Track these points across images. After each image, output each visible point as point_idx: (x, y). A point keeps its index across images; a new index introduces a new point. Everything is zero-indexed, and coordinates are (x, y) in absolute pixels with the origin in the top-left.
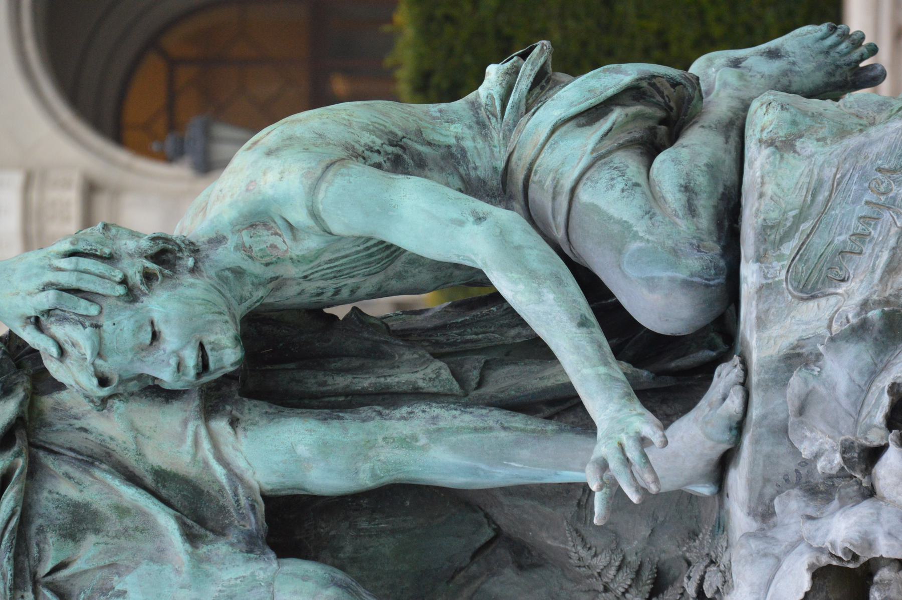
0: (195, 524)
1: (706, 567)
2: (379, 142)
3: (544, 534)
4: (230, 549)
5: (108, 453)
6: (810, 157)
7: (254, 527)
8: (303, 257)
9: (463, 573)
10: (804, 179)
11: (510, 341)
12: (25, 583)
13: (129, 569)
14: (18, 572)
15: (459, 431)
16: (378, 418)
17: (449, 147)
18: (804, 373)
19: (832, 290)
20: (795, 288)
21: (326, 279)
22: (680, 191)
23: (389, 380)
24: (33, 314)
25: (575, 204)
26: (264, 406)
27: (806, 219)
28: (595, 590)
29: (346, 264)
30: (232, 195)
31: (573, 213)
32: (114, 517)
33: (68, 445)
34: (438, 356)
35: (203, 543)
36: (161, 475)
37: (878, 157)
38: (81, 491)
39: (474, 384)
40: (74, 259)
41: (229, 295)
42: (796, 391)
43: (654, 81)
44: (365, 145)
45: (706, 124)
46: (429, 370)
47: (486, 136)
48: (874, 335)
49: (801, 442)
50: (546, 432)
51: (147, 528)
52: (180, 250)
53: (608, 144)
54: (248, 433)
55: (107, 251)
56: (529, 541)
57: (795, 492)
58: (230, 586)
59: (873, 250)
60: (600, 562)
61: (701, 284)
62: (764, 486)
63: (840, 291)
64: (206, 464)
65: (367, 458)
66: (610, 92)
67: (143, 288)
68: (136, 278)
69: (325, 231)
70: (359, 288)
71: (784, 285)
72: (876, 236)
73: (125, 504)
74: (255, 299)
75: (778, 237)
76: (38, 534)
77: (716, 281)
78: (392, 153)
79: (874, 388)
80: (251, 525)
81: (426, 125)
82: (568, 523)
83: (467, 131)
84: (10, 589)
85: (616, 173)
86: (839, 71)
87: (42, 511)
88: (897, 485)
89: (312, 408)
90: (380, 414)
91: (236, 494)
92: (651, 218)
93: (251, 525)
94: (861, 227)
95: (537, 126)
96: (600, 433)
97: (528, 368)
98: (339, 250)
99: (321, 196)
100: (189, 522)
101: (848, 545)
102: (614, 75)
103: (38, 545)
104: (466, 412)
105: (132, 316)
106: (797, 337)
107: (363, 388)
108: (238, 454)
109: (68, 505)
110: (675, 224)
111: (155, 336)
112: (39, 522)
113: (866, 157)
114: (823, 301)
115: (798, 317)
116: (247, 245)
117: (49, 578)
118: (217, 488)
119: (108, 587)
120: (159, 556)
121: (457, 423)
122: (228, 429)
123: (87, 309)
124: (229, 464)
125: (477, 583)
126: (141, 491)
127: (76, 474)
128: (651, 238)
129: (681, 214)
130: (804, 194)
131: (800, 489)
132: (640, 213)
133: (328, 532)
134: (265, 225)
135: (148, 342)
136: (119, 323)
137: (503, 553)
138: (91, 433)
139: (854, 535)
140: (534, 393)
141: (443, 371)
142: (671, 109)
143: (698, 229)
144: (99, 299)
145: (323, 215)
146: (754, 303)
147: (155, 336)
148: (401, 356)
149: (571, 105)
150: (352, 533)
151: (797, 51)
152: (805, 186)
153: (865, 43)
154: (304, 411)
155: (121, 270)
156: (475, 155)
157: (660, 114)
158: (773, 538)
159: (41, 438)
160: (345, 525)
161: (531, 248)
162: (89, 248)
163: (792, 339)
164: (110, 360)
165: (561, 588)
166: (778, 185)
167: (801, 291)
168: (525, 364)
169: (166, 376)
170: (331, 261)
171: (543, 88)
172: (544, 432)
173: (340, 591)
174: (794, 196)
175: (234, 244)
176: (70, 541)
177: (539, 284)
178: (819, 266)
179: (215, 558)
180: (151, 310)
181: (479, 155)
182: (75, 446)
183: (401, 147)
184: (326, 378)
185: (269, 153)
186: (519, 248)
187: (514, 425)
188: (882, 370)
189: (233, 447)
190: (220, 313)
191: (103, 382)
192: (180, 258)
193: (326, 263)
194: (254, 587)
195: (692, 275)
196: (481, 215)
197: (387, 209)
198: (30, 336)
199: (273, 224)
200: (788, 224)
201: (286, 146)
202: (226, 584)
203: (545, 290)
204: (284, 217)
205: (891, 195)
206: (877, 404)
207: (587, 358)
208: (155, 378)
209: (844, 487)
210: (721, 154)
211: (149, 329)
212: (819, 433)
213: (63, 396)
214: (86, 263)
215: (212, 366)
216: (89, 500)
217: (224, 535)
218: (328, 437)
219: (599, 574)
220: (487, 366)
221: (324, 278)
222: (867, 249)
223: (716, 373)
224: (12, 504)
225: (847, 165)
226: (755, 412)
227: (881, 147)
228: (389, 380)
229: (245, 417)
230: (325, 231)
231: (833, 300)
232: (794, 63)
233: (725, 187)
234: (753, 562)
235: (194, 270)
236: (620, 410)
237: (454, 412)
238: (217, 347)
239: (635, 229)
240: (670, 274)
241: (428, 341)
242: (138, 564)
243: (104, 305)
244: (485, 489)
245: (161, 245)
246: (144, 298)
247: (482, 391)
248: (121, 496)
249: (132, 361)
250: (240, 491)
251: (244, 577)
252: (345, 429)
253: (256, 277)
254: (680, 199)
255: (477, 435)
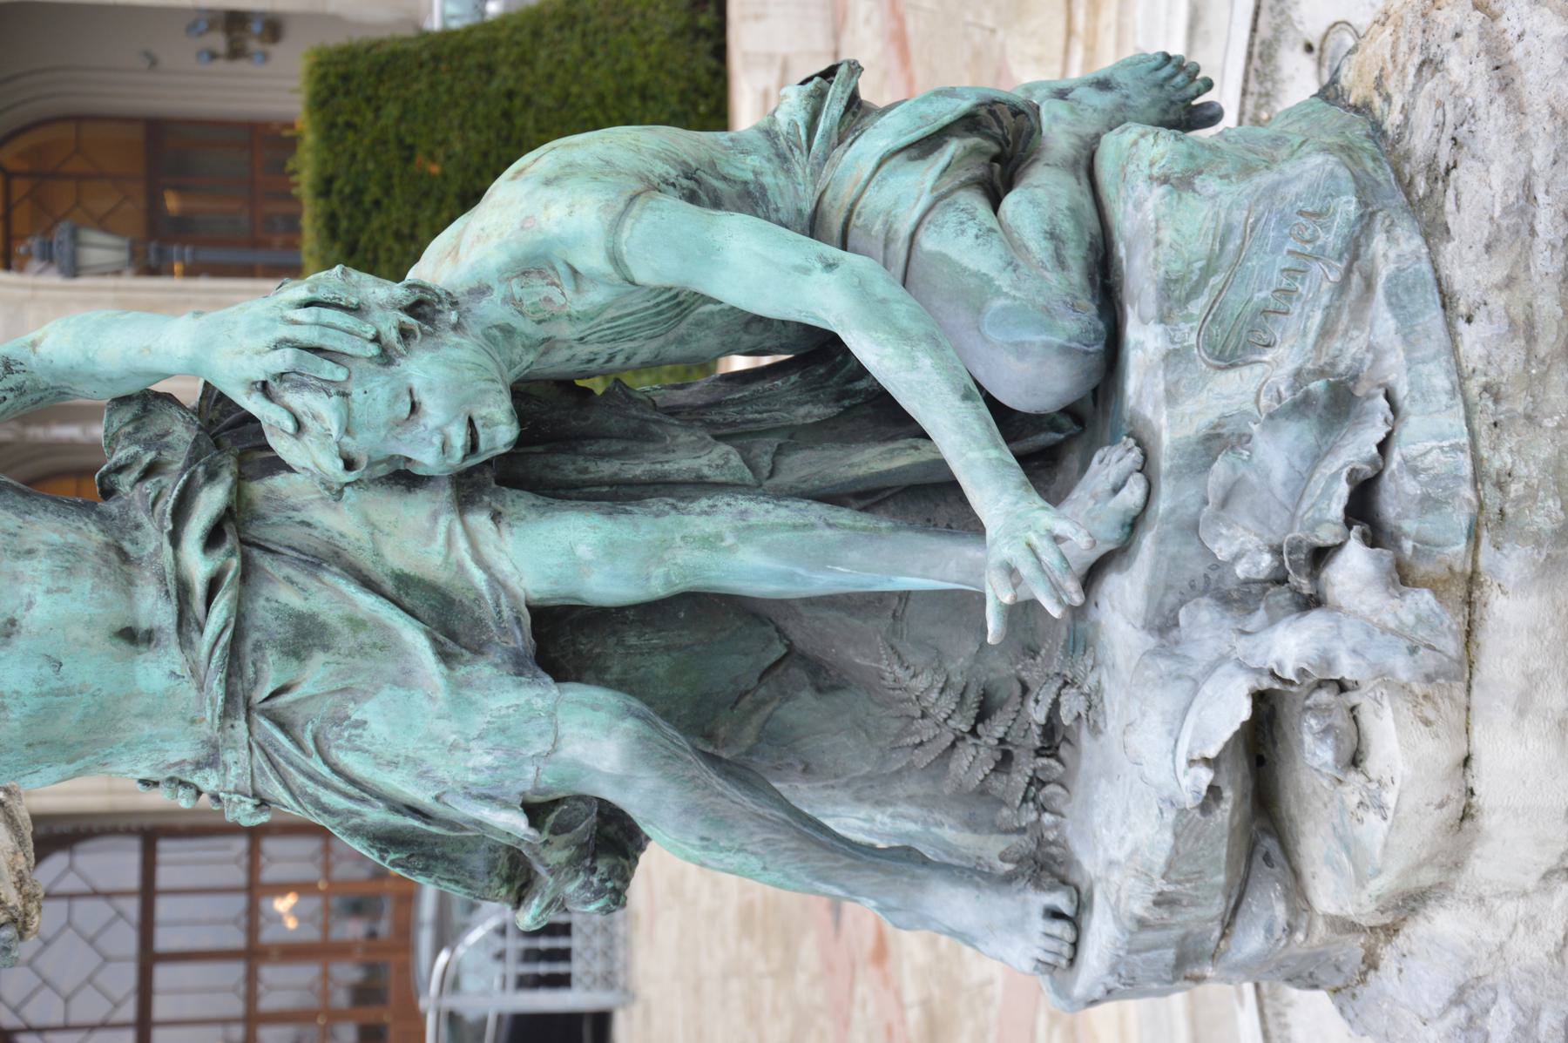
0: (448, 641)
1: (1060, 689)
2: (673, 172)
3: (851, 652)
4: (495, 671)
5: (336, 553)
6: (1214, 197)
7: (520, 644)
8: (585, 314)
9: (748, 697)
10: (1210, 224)
11: (800, 421)
12: (236, 709)
13: (367, 695)
14: (229, 696)
15: (774, 528)
16: (673, 512)
17: (746, 183)
18: (1231, 457)
19: (1256, 357)
20: (1210, 355)
21: (602, 343)
22: (1045, 238)
23: (666, 467)
24: (262, 378)
25: (916, 254)
26: (530, 498)
27: (1215, 272)
28: (908, 716)
29: (629, 323)
30: (501, 235)
31: (913, 264)
32: (346, 631)
33: (286, 543)
34: (718, 438)
35: (460, 663)
36: (403, 580)
37: (1298, 197)
38: (306, 599)
39: (766, 472)
40: (313, 310)
41: (498, 359)
42: (1221, 480)
43: (995, 107)
44: (660, 176)
45: (1050, 162)
46: (714, 455)
47: (788, 171)
48: (1318, 411)
49: (1215, 541)
50: (880, 529)
51: (387, 644)
52: (440, 302)
53: (948, 182)
54: (515, 530)
55: (354, 300)
56: (829, 659)
57: (1205, 600)
58: (501, 717)
59: (1303, 308)
60: (921, 683)
61: (1079, 351)
62: (1165, 594)
63: (1265, 358)
64: (461, 567)
65: (661, 561)
66: (947, 119)
67: (400, 347)
68: (392, 336)
69: (626, 279)
70: (635, 354)
71: (1196, 351)
72: (1305, 293)
73: (360, 616)
74: (525, 364)
75: (1184, 293)
76: (254, 650)
77: (1096, 347)
78: (687, 188)
79: (1317, 476)
80: (516, 642)
81: (719, 155)
82: (882, 638)
83: (767, 165)
84: (220, 717)
85: (964, 217)
86: (1173, 109)
87: (259, 623)
88: (1360, 592)
89: (570, 499)
90: (674, 507)
91: (498, 605)
92: (1015, 271)
93: (516, 642)
94: (1285, 281)
95: (857, 158)
96: (990, 533)
97: (827, 453)
98: (625, 306)
99: (625, 235)
100: (441, 638)
101: (1305, 666)
102: (949, 100)
103: (254, 664)
104: (780, 506)
105: (388, 383)
106: (1218, 413)
107: (635, 476)
108: (502, 555)
109: (290, 615)
110: (1043, 278)
111: (414, 407)
112: (253, 637)
113: (1283, 199)
114: (1246, 371)
115: (1217, 390)
116: (517, 297)
117: (267, 705)
118: (472, 597)
119: (343, 715)
120: (405, 679)
121: (771, 518)
122: (490, 524)
123: (332, 372)
124: (489, 568)
125: (769, 709)
126: (382, 599)
127: (300, 577)
128: (1018, 294)
129: (1049, 266)
130: (1210, 241)
131: (1211, 597)
132: (1001, 264)
133: (590, 650)
134: (540, 272)
135: (405, 415)
136: (371, 391)
137: (798, 673)
138: (316, 528)
139: (1311, 652)
140: (843, 484)
141: (732, 456)
142: (1008, 143)
143: (1071, 284)
144: (346, 360)
145: (627, 260)
146: (1161, 373)
147: (414, 407)
148: (674, 438)
149: (900, 134)
150: (621, 651)
151: (1130, 83)
152: (1211, 232)
153: (1199, 76)
154: (579, 503)
155: (372, 324)
156: (777, 194)
157: (995, 149)
158: (1185, 657)
159: (253, 533)
160: (612, 641)
161: (898, 302)
162: (331, 296)
163: (1212, 416)
164: (359, 437)
165: (868, 714)
166: (1177, 231)
167: (1218, 358)
168: (824, 449)
169: (427, 459)
170: (614, 319)
171: (854, 114)
172: (877, 530)
173: (639, 723)
174: (1198, 244)
175: (501, 296)
176: (293, 659)
177: (912, 346)
178: (1237, 329)
179: (478, 682)
180: (411, 375)
181: (781, 194)
182: (296, 544)
183: (696, 181)
184: (588, 464)
185: (548, 183)
186: (884, 301)
187: (841, 521)
188: (1327, 453)
189: (496, 547)
190: (493, 381)
191: (349, 465)
192: (440, 312)
193: (608, 322)
194: (531, 718)
195: (1070, 340)
196: (831, 261)
197: (709, 254)
198: (254, 405)
199: (550, 272)
200: (1195, 278)
201: (568, 175)
202: (495, 713)
203: (920, 355)
204: (570, 262)
205: (1319, 243)
206: (1326, 494)
207: (975, 439)
208: (409, 460)
209: (1274, 595)
210: (1077, 196)
211: (408, 399)
212: (1241, 529)
213: (279, 481)
214: (330, 315)
215: (482, 445)
216: (315, 609)
217: (482, 654)
218: (616, 536)
219: (918, 698)
220: (780, 451)
221: (600, 341)
222: (1296, 309)
223: (1096, 459)
224: (224, 614)
225: (1261, 208)
226: (1162, 504)
227: (1299, 187)
228: (666, 467)
229: (509, 510)
230: (626, 279)
231: (1258, 369)
232: (1127, 97)
233: (1092, 236)
234: (1164, 685)
235: (457, 327)
236: (1017, 503)
237: (766, 506)
238: (490, 423)
239: (997, 283)
240: (1044, 338)
241: (701, 420)
242: (378, 688)
243: (353, 368)
244: (831, 596)
245: (418, 294)
246: (401, 361)
247: (777, 480)
248: (356, 606)
249: (385, 439)
250: (503, 600)
251: (517, 705)
252: (636, 526)
253: (527, 337)
254: (1046, 248)
255: (796, 534)
